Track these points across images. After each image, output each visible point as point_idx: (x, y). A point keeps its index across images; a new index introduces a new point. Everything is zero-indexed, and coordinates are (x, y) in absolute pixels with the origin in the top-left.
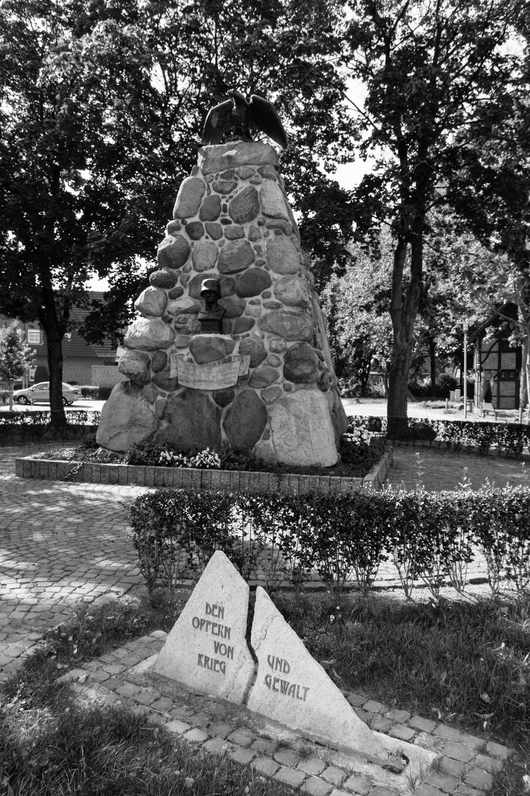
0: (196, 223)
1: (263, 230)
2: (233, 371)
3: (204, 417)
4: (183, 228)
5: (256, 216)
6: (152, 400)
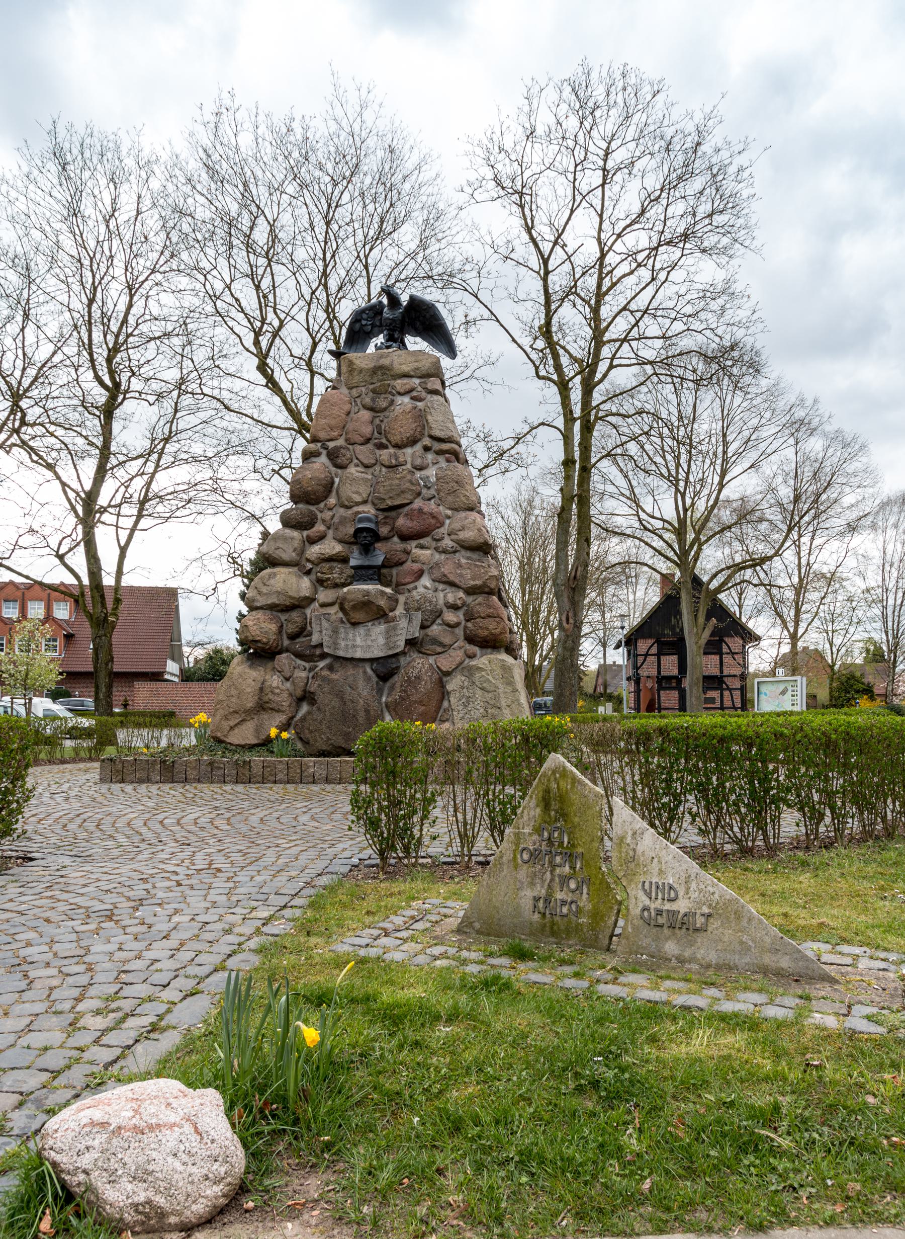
0: (341, 447)
1: (430, 456)
2: (399, 632)
3: (359, 695)
4: (324, 452)
5: (420, 440)
6: (288, 675)
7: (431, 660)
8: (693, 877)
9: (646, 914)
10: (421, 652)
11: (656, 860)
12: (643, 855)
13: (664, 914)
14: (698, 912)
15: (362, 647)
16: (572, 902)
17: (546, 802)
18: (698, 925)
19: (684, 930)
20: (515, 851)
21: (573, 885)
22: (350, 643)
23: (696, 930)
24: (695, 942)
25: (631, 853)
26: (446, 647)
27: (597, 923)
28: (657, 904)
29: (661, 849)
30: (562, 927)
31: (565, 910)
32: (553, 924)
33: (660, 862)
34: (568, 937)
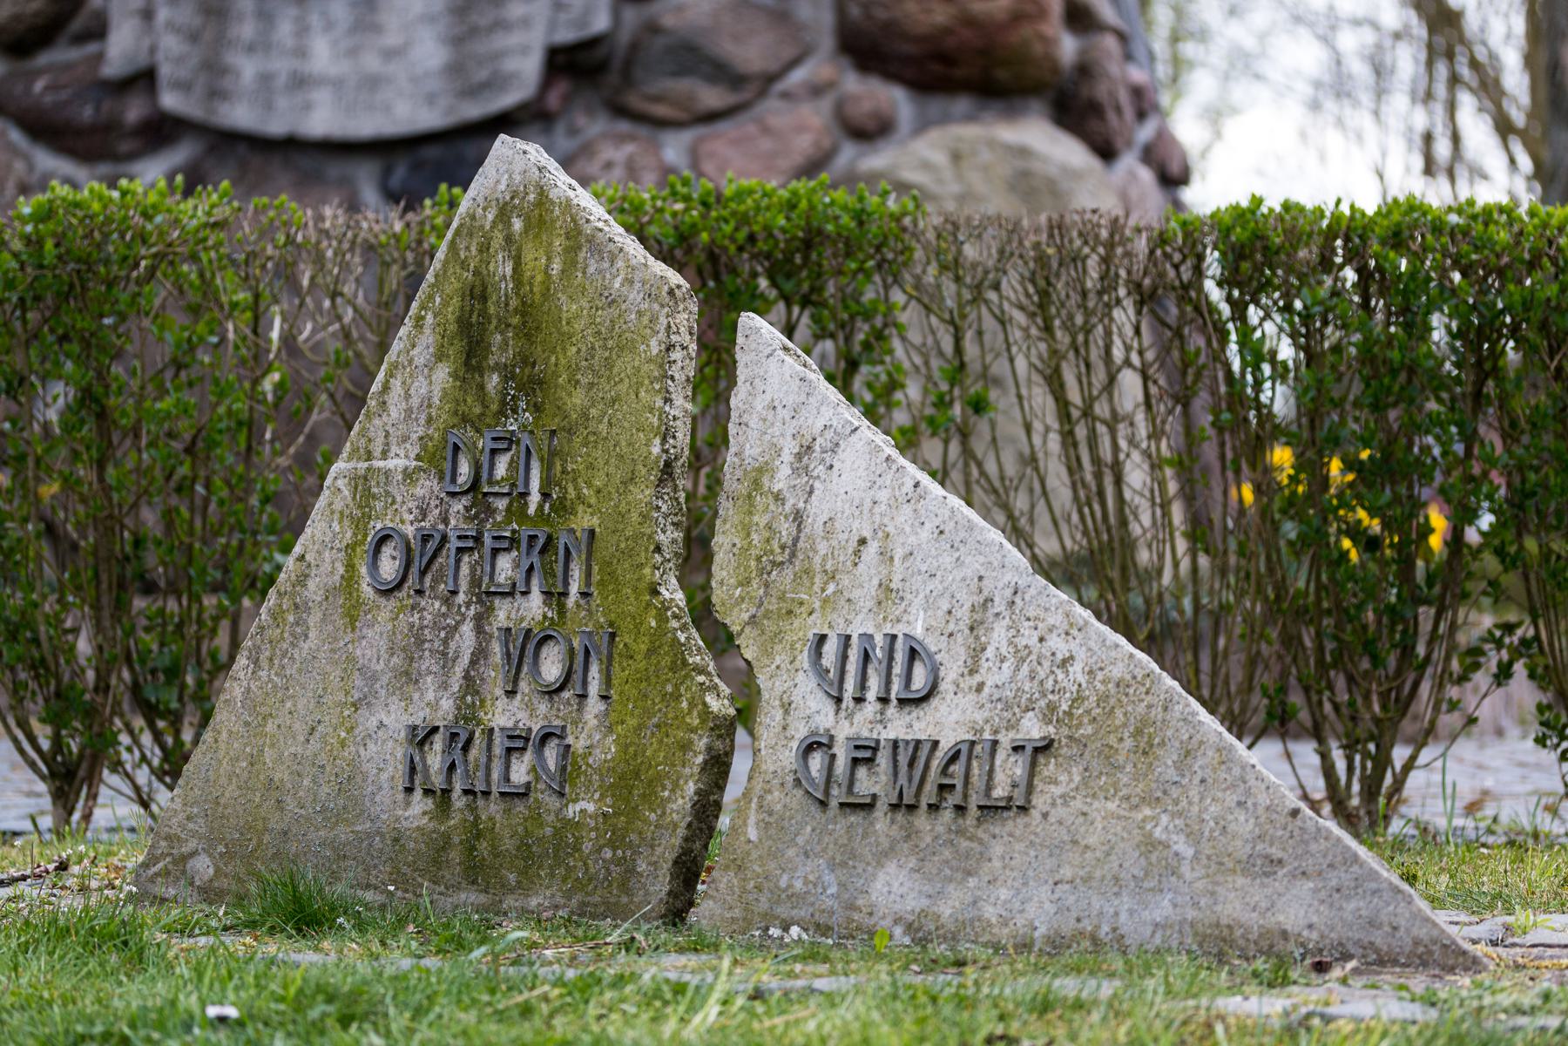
7: (674, 148)
8: (999, 605)
9: (816, 762)
10: (620, 111)
11: (872, 549)
12: (828, 533)
13: (883, 759)
14: (1006, 739)
15: (337, 84)
16: (545, 738)
17: (469, 343)
18: (999, 792)
19: (947, 815)
20: (351, 548)
21: (551, 669)
22: (282, 66)
23: (990, 810)
24: (983, 857)
25: (786, 529)
26: (747, 88)
27: (633, 813)
28: (861, 724)
29: (894, 504)
30: (508, 844)
31: (520, 772)
32: (476, 832)
33: (886, 556)
34: (525, 885)
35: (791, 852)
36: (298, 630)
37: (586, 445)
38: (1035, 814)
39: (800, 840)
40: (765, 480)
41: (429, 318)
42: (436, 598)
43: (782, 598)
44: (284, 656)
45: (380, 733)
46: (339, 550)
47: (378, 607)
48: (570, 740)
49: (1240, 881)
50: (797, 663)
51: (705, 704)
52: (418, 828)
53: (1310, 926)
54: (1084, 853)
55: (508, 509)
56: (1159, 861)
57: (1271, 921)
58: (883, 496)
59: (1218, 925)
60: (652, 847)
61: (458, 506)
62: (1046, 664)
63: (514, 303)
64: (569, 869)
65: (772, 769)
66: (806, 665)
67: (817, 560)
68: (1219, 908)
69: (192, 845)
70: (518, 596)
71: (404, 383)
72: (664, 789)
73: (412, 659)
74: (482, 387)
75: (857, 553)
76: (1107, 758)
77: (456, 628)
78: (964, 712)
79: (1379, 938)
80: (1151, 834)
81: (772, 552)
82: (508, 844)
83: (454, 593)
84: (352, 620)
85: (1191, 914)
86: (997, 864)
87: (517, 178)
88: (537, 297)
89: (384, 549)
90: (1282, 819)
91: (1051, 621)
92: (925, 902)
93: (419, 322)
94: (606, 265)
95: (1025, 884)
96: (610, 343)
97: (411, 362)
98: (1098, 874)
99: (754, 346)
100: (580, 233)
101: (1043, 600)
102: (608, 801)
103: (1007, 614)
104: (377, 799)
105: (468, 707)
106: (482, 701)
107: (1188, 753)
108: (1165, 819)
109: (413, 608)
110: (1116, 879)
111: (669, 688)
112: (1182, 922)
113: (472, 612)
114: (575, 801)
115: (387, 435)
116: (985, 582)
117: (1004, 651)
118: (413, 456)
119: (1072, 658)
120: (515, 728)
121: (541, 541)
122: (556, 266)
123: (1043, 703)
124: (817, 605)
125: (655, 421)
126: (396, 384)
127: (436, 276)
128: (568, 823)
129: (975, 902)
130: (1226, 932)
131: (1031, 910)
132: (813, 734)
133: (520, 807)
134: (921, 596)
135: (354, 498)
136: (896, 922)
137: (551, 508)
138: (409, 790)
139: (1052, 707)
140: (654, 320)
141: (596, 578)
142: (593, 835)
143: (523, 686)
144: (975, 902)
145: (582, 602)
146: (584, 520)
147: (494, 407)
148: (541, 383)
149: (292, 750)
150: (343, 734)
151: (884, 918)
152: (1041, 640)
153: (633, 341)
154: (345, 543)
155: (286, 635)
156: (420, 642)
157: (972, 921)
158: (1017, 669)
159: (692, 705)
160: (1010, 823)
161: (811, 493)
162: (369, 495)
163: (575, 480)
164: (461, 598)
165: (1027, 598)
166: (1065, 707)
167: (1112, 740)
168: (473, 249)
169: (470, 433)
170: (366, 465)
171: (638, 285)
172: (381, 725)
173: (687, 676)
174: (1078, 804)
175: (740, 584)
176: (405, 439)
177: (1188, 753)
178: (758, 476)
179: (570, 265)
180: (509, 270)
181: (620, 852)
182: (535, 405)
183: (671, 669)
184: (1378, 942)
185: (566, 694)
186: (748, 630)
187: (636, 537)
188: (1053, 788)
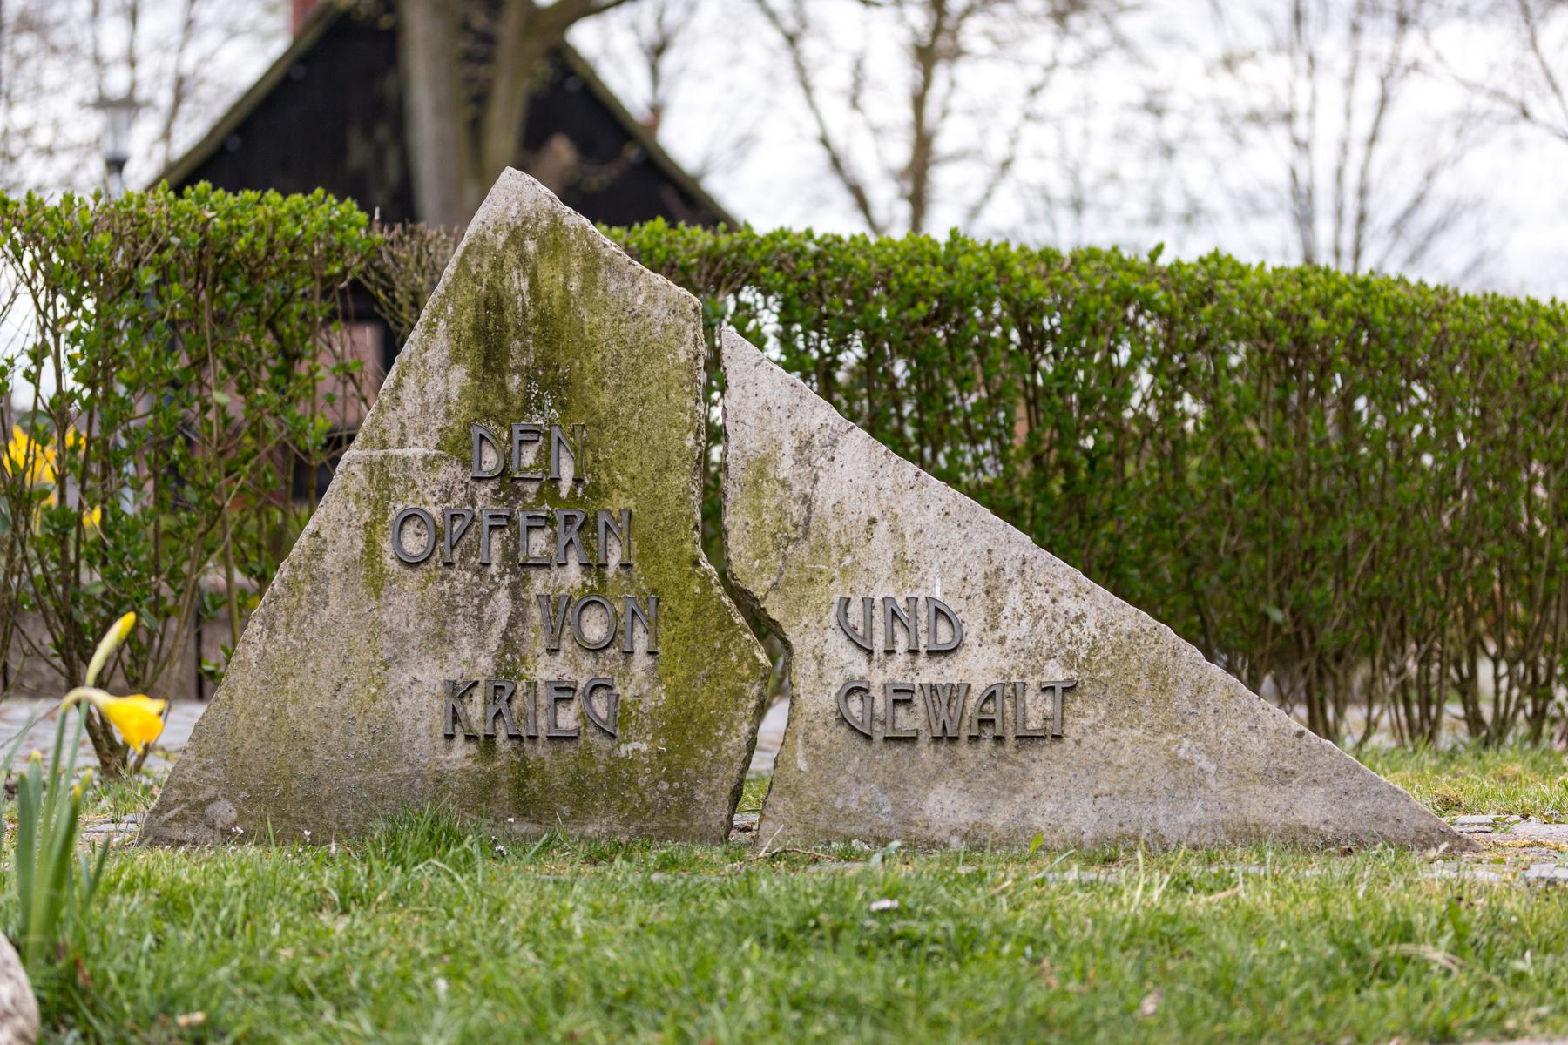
8: (1010, 572)
11: (882, 528)
13: (918, 699)
14: (1033, 682)
17: (487, 345)
19: (987, 745)
20: (370, 526)
21: (595, 628)
23: (1028, 739)
24: (1027, 777)
25: (796, 511)
27: (689, 751)
28: (896, 670)
30: (559, 781)
31: (568, 719)
32: (523, 771)
33: (897, 533)
35: (842, 779)
36: (317, 598)
37: (617, 438)
38: (1069, 741)
39: (849, 769)
40: (770, 470)
41: (442, 325)
42: (467, 569)
43: (801, 568)
44: (303, 620)
45: (414, 688)
46: (358, 528)
47: (405, 578)
48: (618, 690)
49: (1260, 789)
50: (825, 623)
51: (754, 657)
52: (462, 770)
53: (1326, 822)
54: (1117, 772)
55: (539, 493)
56: (1187, 776)
57: (1291, 819)
58: (887, 483)
59: (1246, 824)
60: (710, 779)
61: (485, 489)
62: (1061, 621)
63: (532, 314)
64: (625, 800)
65: (813, 710)
66: (834, 624)
67: (831, 536)
68: (1244, 811)
69: (211, 791)
70: (555, 567)
71: (418, 381)
72: (718, 729)
73: (444, 623)
74: (503, 386)
75: (869, 530)
76: (1128, 695)
77: (490, 595)
78: (990, 660)
79: (1386, 829)
80: (1176, 755)
81: (786, 530)
82: (559, 781)
83: (488, 565)
84: (377, 591)
85: (1221, 817)
86: (1039, 782)
87: (528, 206)
88: (557, 310)
89: (406, 526)
90: (1290, 740)
91: (1061, 586)
92: (977, 816)
93: (431, 328)
94: (627, 284)
95: (1068, 798)
96: (636, 352)
97: (424, 363)
98: (1133, 787)
99: (740, 356)
100: (598, 256)
101: (1050, 569)
102: (661, 741)
103: (1019, 580)
104: (416, 745)
105: (508, 663)
106: (523, 659)
107: (1199, 690)
108: (1186, 742)
109: (442, 578)
110: (1150, 791)
111: (718, 645)
112: (1215, 823)
113: (507, 580)
114: (628, 742)
115: (403, 426)
116: (994, 554)
117: (1020, 610)
118: (432, 445)
119: (1084, 615)
120: (560, 680)
121: (579, 521)
122: (575, 284)
123: (1063, 652)
124: (836, 574)
125: (688, 419)
126: (410, 383)
127: (447, 288)
128: (620, 761)
129: (1024, 814)
130: (1253, 829)
131: (1077, 819)
132: (849, 681)
133: (569, 748)
134: (936, 566)
135: (370, 482)
136: (952, 833)
137: (585, 491)
138: (450, 737)
139: (1072, 656)
140: (680, 332)
141: (635, 552)
142: (648, 770)
143: (566, 644)
144: (1024, 814)
145: (623, 572)
146: (619, 503)
147: (518, 404)
148: (566, 384)
149: (319, 704)
150: (373, 690)
151: (940, 829)
152: (1054, 601)
153: (660, 350)
154: (363, 521)
155: (303, 603)
156: (452, 608)
157: (1023, 829)
158: (1035, 625)
159: (741, 659)
160: (1047, 749)
161: (816, 480)
162: (386, 480)
163: (607, 468)
164: (494, 569)
165: (1035, 567)
166: (1083, 655)
167: (1130, 680)
168: (486, 267)
169: (493, 426)
170: (382, 452)
171: (661, 303)
172: (415, 681)
173: (734, 634)
174: (1107, 732)
175: (758, 556)
176: (423, 430)
177: (1199, 690)
178: (761, 467)
179: (589, 283)
180: (525, 285)
181: (676, 785)
182: (561, 403)
183: (718, 629)
184: (1386, 832)
185: (611, 651)
186: (771, 595)
187: (673, 518)
188: (1082, 720)
